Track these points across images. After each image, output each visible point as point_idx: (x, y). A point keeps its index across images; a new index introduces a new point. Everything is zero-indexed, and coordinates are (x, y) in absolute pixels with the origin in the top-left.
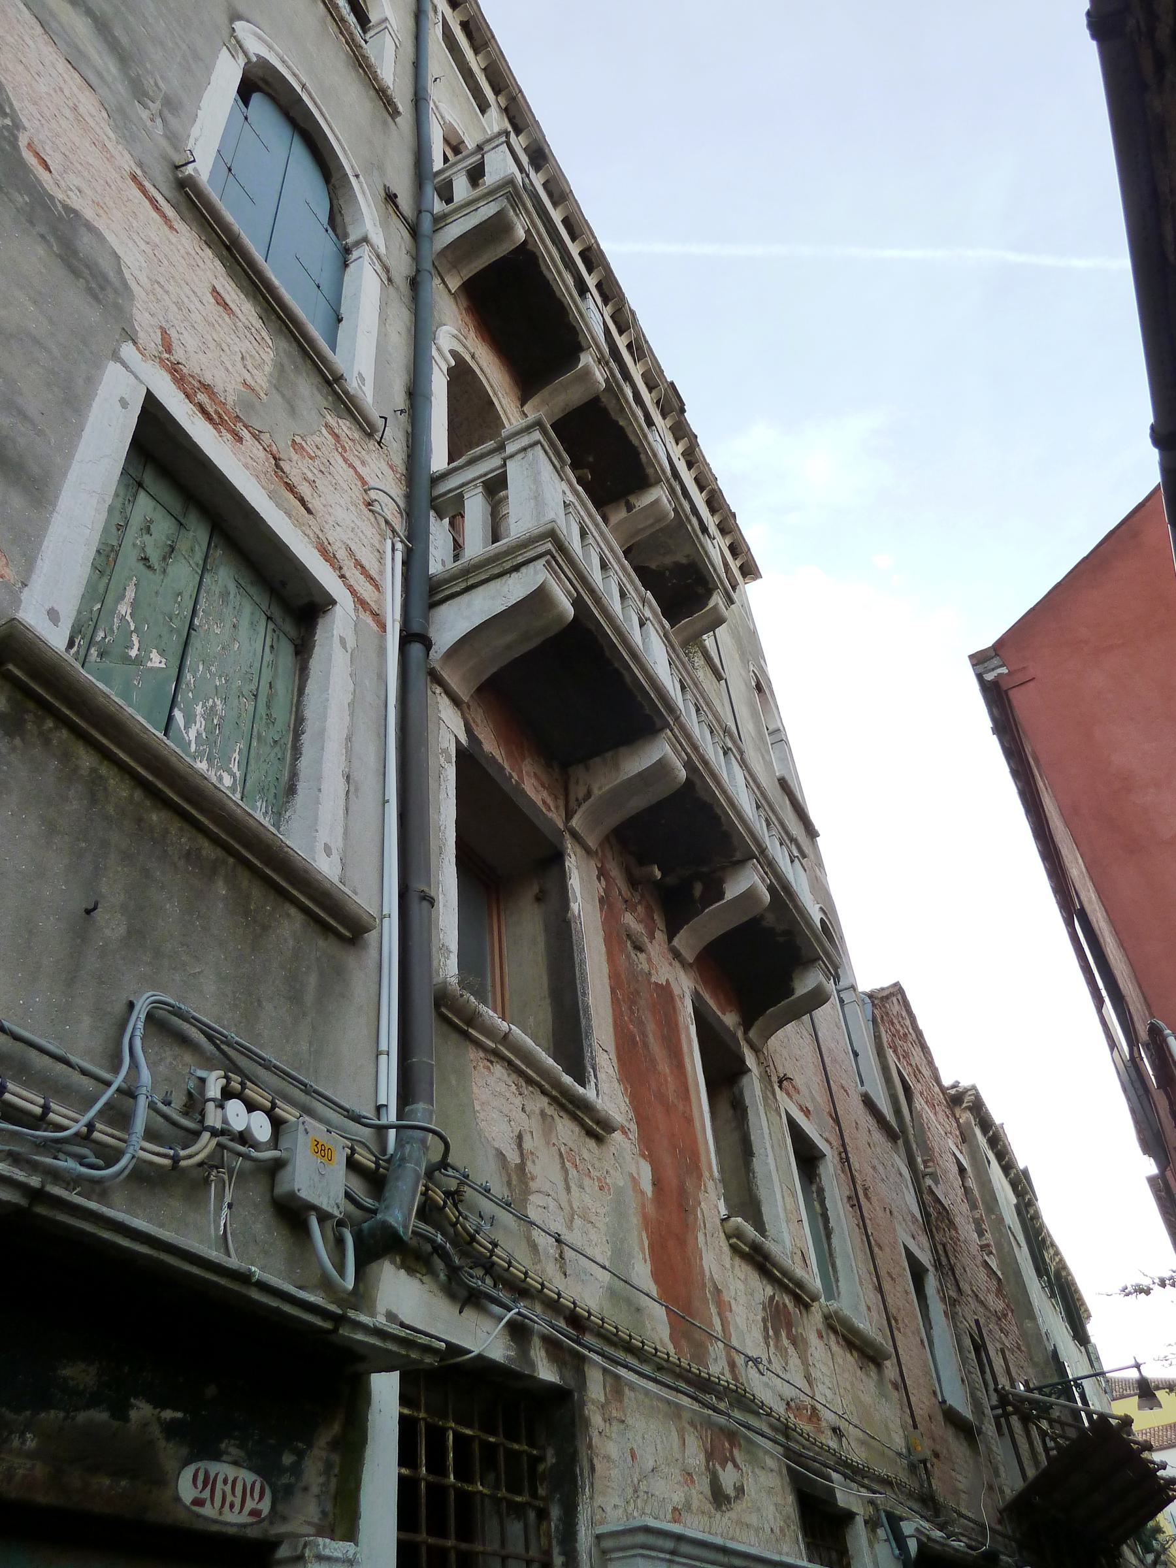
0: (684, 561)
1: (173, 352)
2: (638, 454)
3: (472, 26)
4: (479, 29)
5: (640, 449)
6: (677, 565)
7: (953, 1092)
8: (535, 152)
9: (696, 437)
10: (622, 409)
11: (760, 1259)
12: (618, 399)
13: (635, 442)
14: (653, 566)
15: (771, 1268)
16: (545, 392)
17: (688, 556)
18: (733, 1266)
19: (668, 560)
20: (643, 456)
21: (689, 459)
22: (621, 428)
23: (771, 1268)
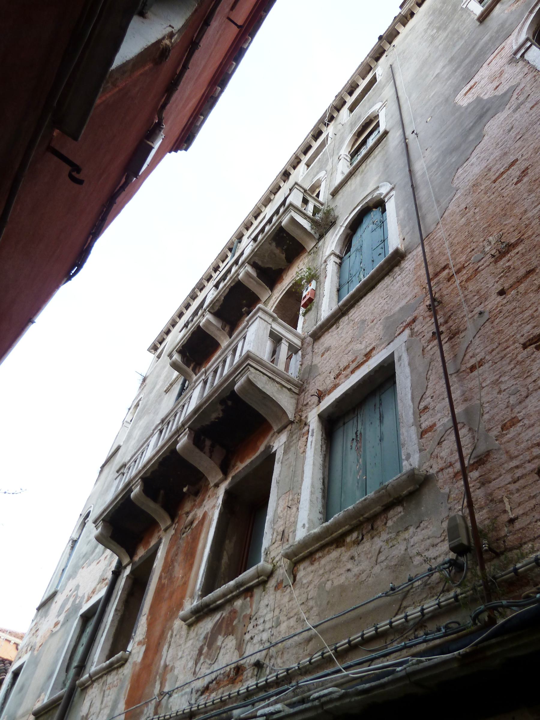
0: (274, 244)
1: (192, 628)
2: (232, 287)
3: (255, 215)
4: (255, 212)
5: (230, 287)
6: (277, 246)
7: (318, 217)
8: (285, 176)
9: (395, 18)
10: (217, 300)
11: (206, 610)
12: (215, 303)
13: (228, 290)
14: (283, 256)
15: (214, 605)
16: (217, 339)
17: (270, 244)
18: (234, 652)
19: (277, 251)
20: (232, 285)
21: (409, 16)
22: (225, 298)
23: (214, 605)
